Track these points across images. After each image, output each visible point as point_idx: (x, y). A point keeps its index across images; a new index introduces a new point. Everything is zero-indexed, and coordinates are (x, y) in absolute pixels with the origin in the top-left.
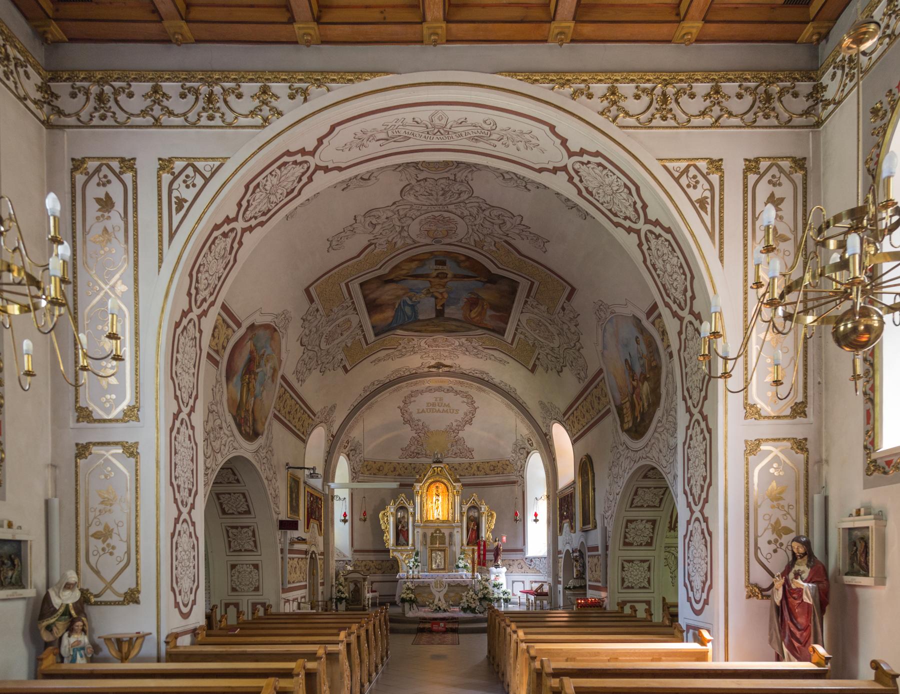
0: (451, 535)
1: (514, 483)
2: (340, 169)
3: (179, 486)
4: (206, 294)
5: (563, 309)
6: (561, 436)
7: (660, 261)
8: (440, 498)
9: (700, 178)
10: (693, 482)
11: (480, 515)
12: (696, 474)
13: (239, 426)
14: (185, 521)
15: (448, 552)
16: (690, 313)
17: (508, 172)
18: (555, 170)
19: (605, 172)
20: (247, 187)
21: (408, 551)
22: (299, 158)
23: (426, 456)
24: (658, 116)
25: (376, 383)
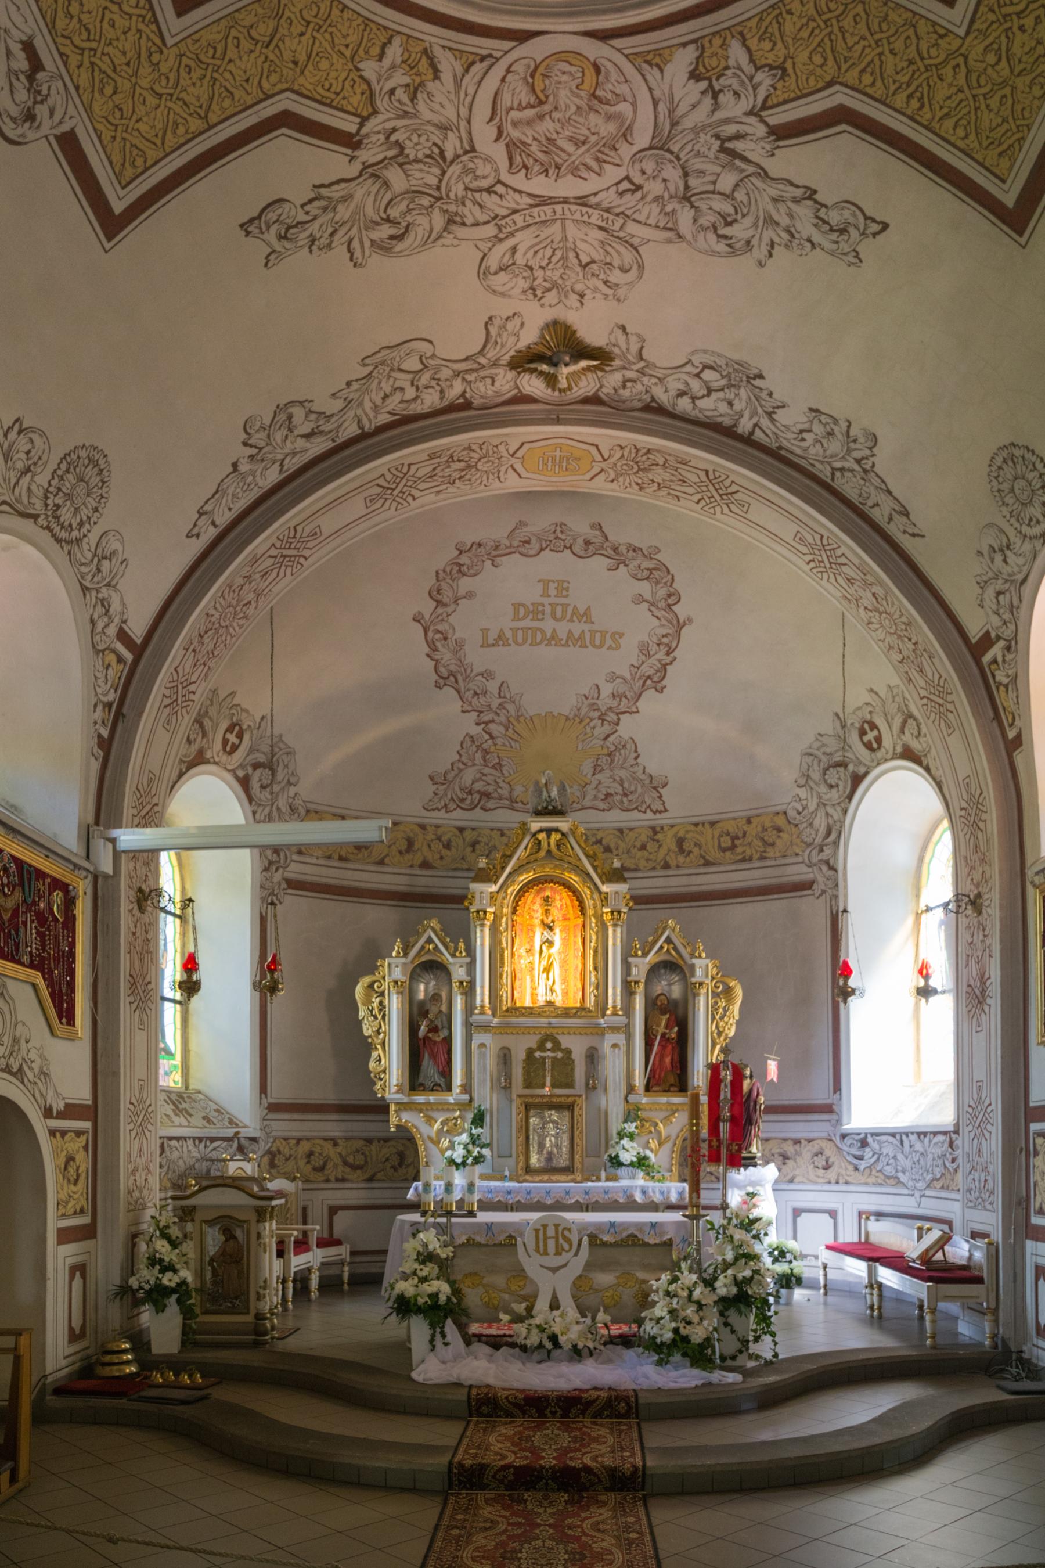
0: (593, 1057)
1: (808, 885)
8: (557, 937)
11: (691, 990)
15: (583, 1110)
21: (444, 1107)
23: (513, 803)
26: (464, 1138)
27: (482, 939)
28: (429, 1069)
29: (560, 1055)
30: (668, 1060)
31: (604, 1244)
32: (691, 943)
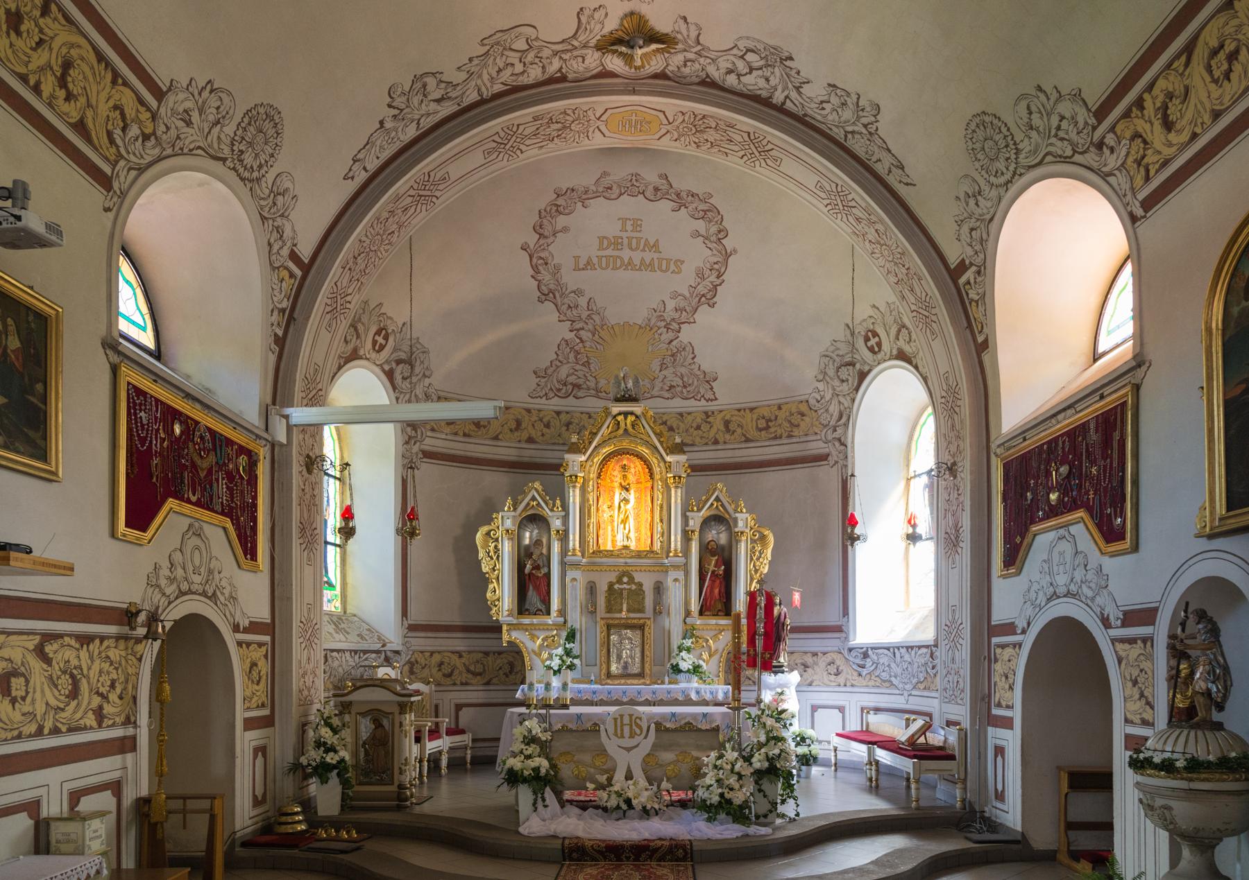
0: (659, 589)
1: (823, 458)
8: (632, 496)
11: (734, 538)
15: (650, 631)
21: (546, 627)
23: (597, 393)
26: (560, 651)
27: (574, 497)
28: (533, 597)
29: (634, 587)
30: (717, 591)
31: (667, 730)
32: (735, 501)
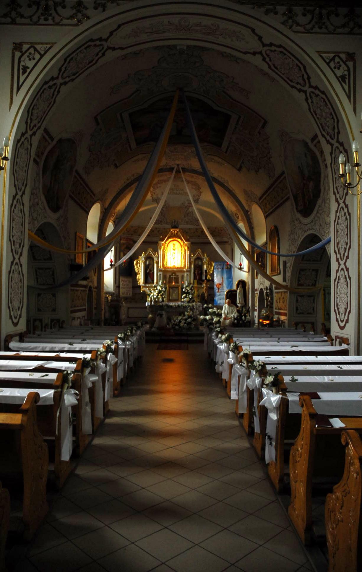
1: (226, 242)
2: (122, 49)
3: (14, 242)
4: (35, 122)
5: (260, 133)
6: (258, 215)
7: (319, 110)
9: (341, 63)
10: (340, 246)
12: (342, 241)
13: (48, 203)
14: (17, 263)
16: (333, 145)
17: (225, 52)
18: (254, 54)
19: (285, 56)
20: (65, 60)
22: (98, 43)
23: (167, 223)
24: (316, 26)
25: (135, 175)
27: (161, 252)
